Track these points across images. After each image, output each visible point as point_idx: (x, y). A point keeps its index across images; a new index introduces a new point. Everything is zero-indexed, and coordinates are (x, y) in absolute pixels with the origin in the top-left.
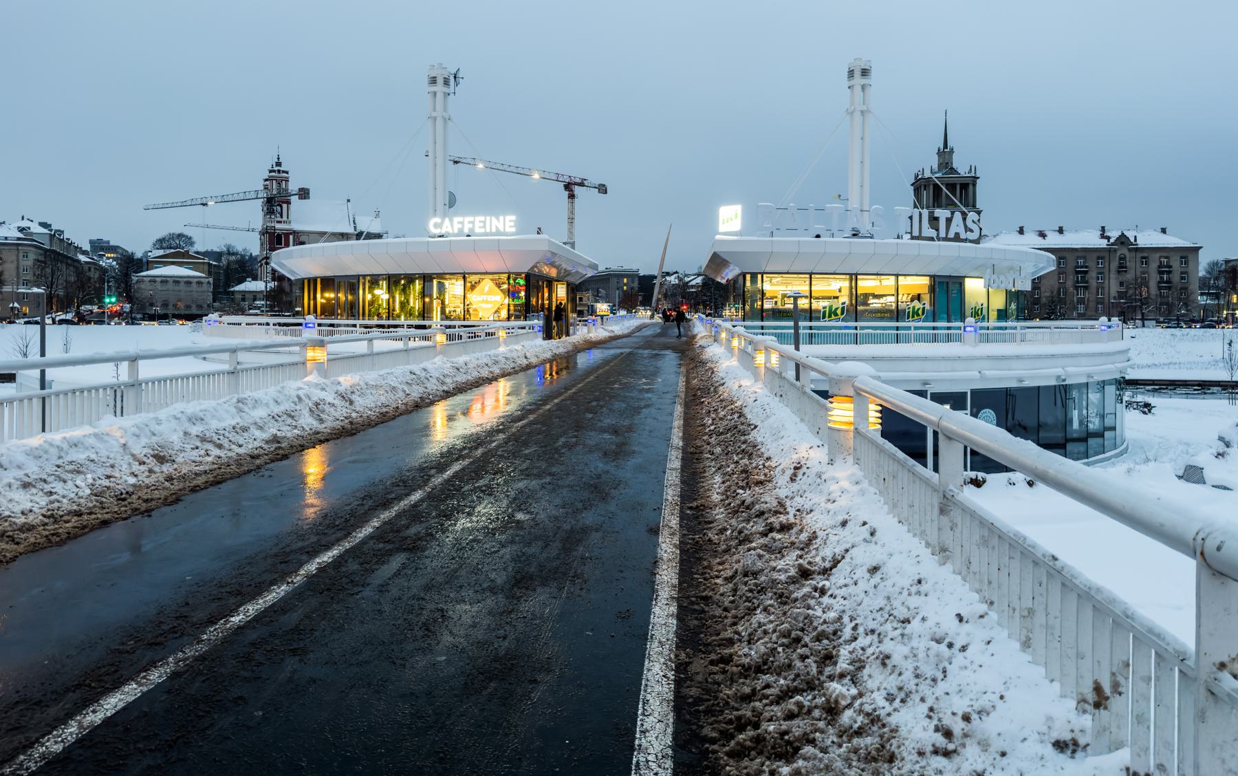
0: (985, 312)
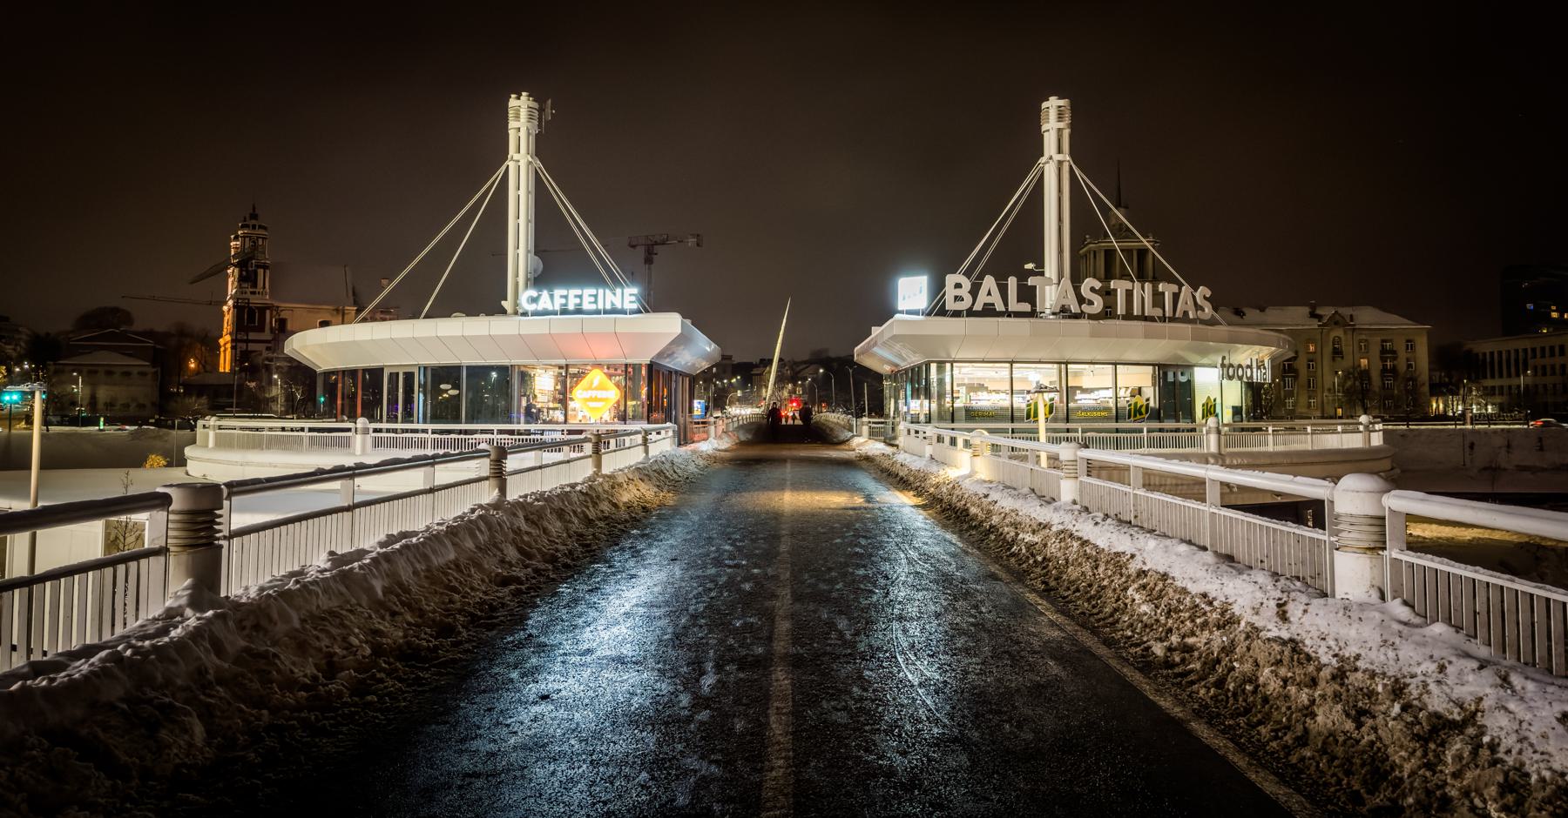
0: (1218, 410)
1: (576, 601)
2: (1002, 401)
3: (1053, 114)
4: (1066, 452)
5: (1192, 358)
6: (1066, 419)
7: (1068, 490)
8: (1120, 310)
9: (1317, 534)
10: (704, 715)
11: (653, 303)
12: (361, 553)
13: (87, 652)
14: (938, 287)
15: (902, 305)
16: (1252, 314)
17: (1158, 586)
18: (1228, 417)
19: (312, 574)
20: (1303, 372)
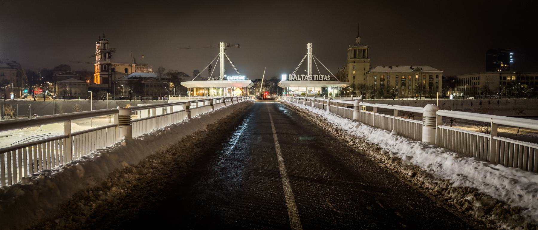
20: (407, 84)
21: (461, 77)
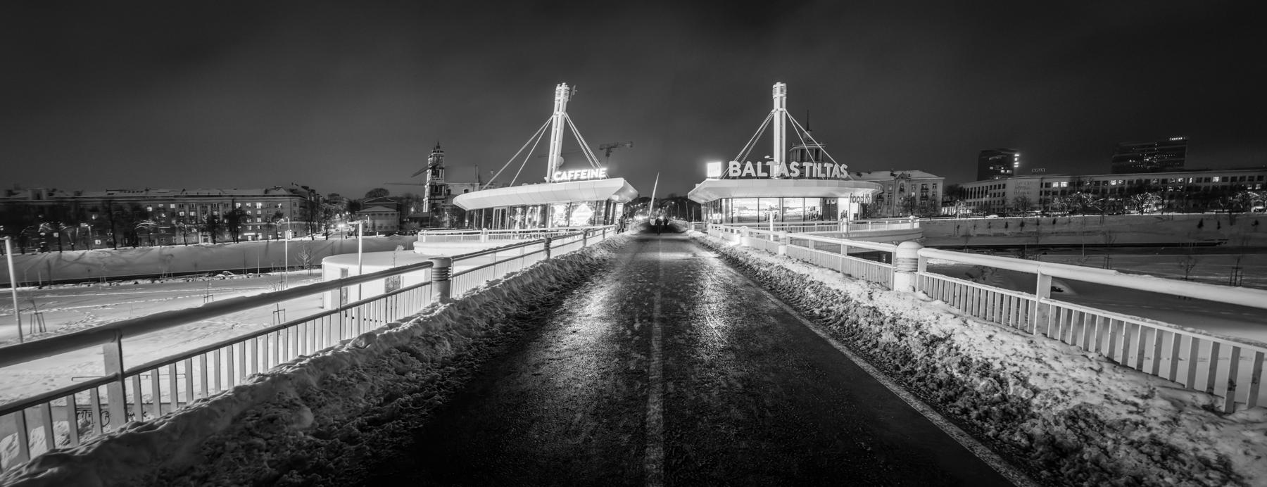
1: (581, 296)
2: (754, 214)
3: (778, 90)
4: (781, 234)
5: (838, 194)
6: (783, 221)
7: (782, 250)
8: (807, 175)
9: (888, 266)
10: (637, 338)
11: (611, 175)
12: (498, 281)
13: (407, 319)
14: (726, 167)
15: (709, 175)
16: (864, 175)
17: (818, 287)
18: (852, 218)
19: (481, 290)
20: (886, 199)
21: (968, 186)
